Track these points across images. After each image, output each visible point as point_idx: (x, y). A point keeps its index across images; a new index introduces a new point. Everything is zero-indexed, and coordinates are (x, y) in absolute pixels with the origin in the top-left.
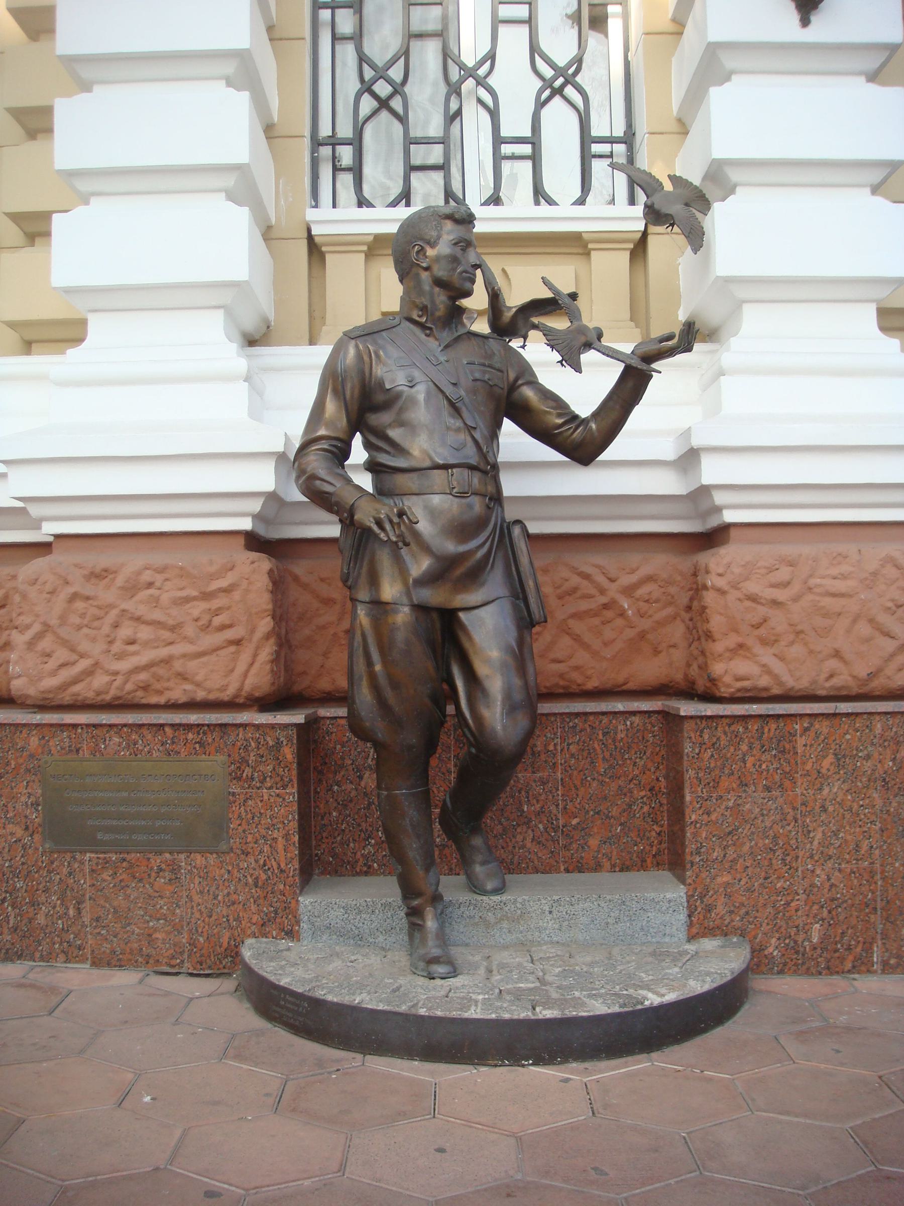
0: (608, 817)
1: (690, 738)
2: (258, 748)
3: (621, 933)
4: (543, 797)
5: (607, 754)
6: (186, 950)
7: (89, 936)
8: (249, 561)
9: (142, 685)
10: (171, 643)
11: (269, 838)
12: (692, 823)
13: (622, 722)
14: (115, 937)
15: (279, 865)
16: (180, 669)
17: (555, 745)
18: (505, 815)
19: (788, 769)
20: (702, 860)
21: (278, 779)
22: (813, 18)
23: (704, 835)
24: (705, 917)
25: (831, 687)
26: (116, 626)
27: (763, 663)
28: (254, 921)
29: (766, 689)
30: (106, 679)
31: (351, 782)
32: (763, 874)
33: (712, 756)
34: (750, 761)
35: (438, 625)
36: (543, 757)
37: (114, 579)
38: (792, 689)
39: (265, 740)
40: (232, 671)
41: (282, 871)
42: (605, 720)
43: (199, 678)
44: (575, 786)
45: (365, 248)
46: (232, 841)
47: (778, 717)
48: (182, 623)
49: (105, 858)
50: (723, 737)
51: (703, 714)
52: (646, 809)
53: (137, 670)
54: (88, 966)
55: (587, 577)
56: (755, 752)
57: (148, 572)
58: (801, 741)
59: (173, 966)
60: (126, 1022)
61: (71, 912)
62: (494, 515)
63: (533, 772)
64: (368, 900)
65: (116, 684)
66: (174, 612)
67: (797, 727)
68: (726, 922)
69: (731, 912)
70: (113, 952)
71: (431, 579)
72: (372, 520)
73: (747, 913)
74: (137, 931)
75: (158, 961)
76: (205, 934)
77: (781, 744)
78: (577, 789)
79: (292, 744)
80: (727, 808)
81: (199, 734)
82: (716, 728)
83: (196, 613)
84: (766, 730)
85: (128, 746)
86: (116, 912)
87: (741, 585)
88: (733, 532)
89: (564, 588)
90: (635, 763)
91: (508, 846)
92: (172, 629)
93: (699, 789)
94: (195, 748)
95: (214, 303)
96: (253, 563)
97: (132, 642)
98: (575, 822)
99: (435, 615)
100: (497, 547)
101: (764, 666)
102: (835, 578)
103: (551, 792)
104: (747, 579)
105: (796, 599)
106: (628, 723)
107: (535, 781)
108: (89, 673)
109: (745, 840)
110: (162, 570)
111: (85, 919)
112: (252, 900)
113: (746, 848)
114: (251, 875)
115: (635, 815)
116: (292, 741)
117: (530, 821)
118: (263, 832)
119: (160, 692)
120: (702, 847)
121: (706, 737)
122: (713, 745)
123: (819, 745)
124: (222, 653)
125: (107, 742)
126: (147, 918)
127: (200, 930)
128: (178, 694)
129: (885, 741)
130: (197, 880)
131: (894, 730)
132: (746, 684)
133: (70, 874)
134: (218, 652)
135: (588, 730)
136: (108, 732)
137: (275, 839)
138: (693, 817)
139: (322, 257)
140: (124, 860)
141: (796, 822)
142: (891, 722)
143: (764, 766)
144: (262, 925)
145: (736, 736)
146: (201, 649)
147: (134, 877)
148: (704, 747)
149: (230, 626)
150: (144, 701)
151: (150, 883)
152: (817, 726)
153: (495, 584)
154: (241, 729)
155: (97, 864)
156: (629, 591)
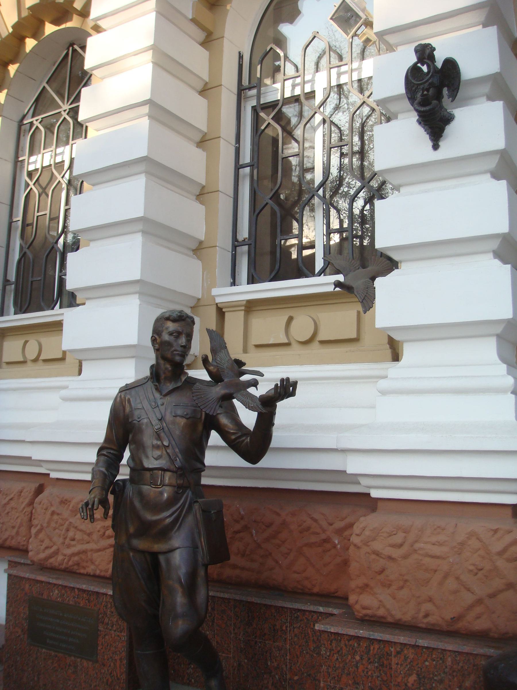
1: (324, 644)
5: (315, 638)
10: (88, 543)
17: (286, 627)
19: (385, 678)
21: (118, 627)
22: (441, 143)
25: (427, 623)
29: (382, 617)
33: (337, 659)
34: (361, 667)
38: (400, 620)
41: (118, 679)
45: (243, 308)
50: (344, 647)
51: (329, 630)
53: (74, 555)
55: (315, 521)
56: (364, 662)
58: (394, 661)
61: (36, 678)
62: (185, 496)
63: (274, 642)
67: (392, 650)
81: (88, 595)
82: (340, 641)
84: (372, 648)
87: (369, 544)
88: (380, 504)
93: (329, 680)
95: (128, 356)
97: (73, 539)
98: (296, 678)
101: (381, 601)
102: (434, 544)
103: (283, 656)
104: (374, 539)
105: (405, 557)
107: (274, 647)
108: (56, 553)
119: (84, 568)
121: (334, 645)
122: (338, 652)
123: (407, 665)
129: (454, 671)
130: (84, 675)
131: (461, 664)
135: (305, 621)
137: (116, 660)
139: (223, 313)
142: (458, 658)
143: (370, 673)
145: (353, 649)
150: (78, 571)
152: (405, 652)
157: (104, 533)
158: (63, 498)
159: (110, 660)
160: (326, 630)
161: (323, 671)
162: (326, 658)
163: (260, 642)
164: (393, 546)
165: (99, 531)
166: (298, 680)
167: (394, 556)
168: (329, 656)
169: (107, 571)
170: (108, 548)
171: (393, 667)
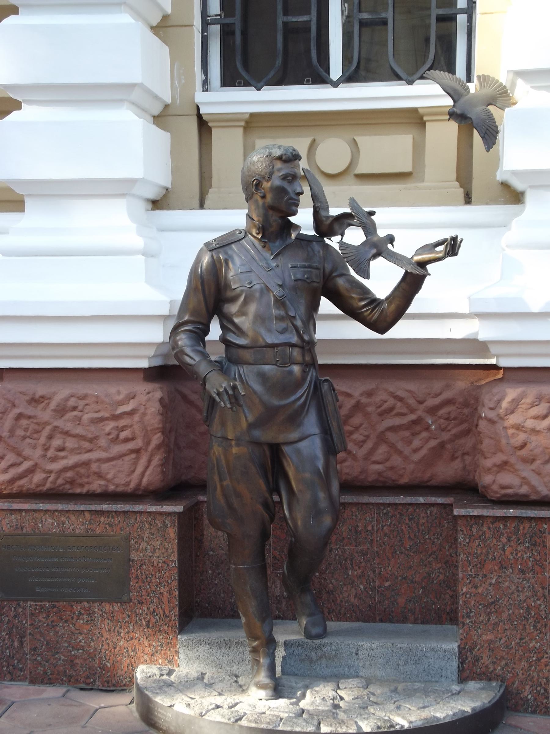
0: (412, 582)
2: (150, 529)
3: (408, 673)
4: (363, 565)
5: (412, 536)
6: (98, 672)
7: (29, 662)
8: (145, 392)
9: (69, 480)
11: (157, 592)
12: (463, 594)
13: (424, 511)
14: (47, 662)
15: (164, 612)
16: (97, 470)
17: (373, 526)
18: (335, 577)
20: (472, 622)
21: (164, 551)
23: (473, 603)
24: (474, 665)
26: (50, 437)
27: (523, 476)
28: (146, 652)
29: (525, 496)
30: (44, 475)
31: (222, 549)
32: (519, 636)
33: (479, 545)
34: (508, 549)
35: (268, 453)
36: (363, 535)
37: (49, 404)
39: (155, 523)
40: (133, 471)
41: (166, 616)
42: (411, 509)
43: (109, 476)
44: (388, 558)
46: (131, 594)
47: (530, 519)
48: (97, 436)
49: (41, 605)
50: (488, 531)
51: (471, 514)
52: (441, 577)
53: (66, 469)
54: (27, 683)
56: (512, 544)
57: (73, 399)
59: (88, 684)
60: (50, 725)
61: (16, 644)
63: (356, 546)
64: (226, 639)
65: (50, 479)
66: (92, 428)
68: (491, 670)
69: (494, 663)
70: (45, 672)
71: (261, 422)
72: (215, 390)
73: (506, 664)
74: (63, 658)
75: (77, 680)
76: (111, 661)
77: (533, 540)
78: (389, 560)
79: (174, 526)
80: (490, 584)
81: (108, 517)
82: (482, 525)
83: (108, 429)
84: (521, 528)
85: (58, 525)
86: (48, 644)
89: (383, 408)
90: (434, 542)
91: (337, 600)
92: (91, 441)
93: (469, 569)
94: (106, 528)
96: (148, 393)
98: (387, 584)
99: (266, 448)
100: (311, 397)
101: (524, 478)
106: (428, 512)
107: (357, 552)
108: (31, 471)
109: (505, 609)
110: (84, 397)
111: (25, 649)
112: (145, 637)
113: (505, 615)
114: (145, 619)
115: (433, 582)
116: (174, 524)
117: (353, 582)
118: (154, 588)
119: (82, 485)
120: (471, 612)
122: (480, 537)
124: (127, 458)
125: (44, 522)
126: (70, 649)
127: (108, 658)
128: (97, 486)
132: (509, 491)
133: (16, 616)
134: (123, 458)
135: (398, 516)
136: (44, 515)
137: (162, 594)
138: (464, 589)
140: (54, 607)
141: (545, 598)
143: (519, 555)
144: (152, 655)
145: (498, 531)
146: (112, 456)
147: (62, 619)
148: (473, 538)
149: (133, 439)
150: (70, 491)
151: (73, 624)
153: (311, 424)
154: (138, 515)
155: (35, 609)
156: (432, 411)
157: (118, 436)
158: (34, 394)
159: (152, 595)
160: (468, 514)
161: (462, 561)
162: (464, 545)
163: (337, 549)
164: (536, 418)
165: (109, 434)
166: (390, 586)
167: (538, 428)
168: (468, 543)
169: (128, 485)
170: (128, 454)
171: (548, 545)
